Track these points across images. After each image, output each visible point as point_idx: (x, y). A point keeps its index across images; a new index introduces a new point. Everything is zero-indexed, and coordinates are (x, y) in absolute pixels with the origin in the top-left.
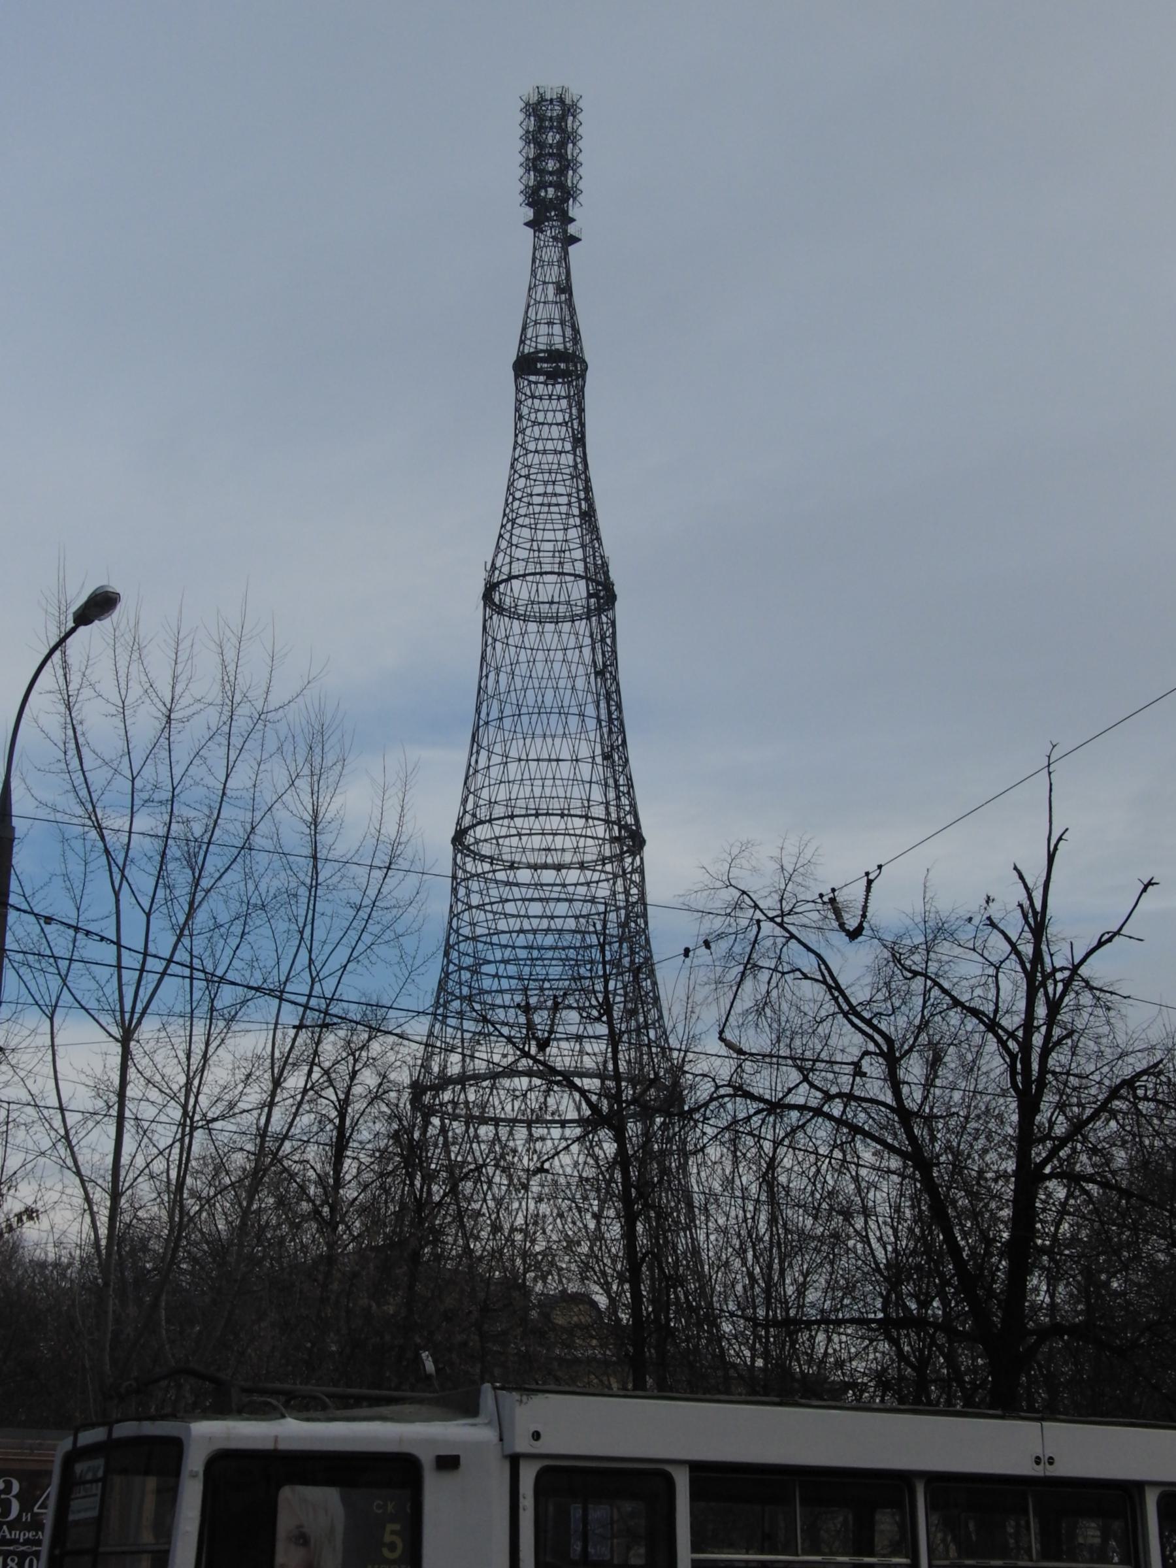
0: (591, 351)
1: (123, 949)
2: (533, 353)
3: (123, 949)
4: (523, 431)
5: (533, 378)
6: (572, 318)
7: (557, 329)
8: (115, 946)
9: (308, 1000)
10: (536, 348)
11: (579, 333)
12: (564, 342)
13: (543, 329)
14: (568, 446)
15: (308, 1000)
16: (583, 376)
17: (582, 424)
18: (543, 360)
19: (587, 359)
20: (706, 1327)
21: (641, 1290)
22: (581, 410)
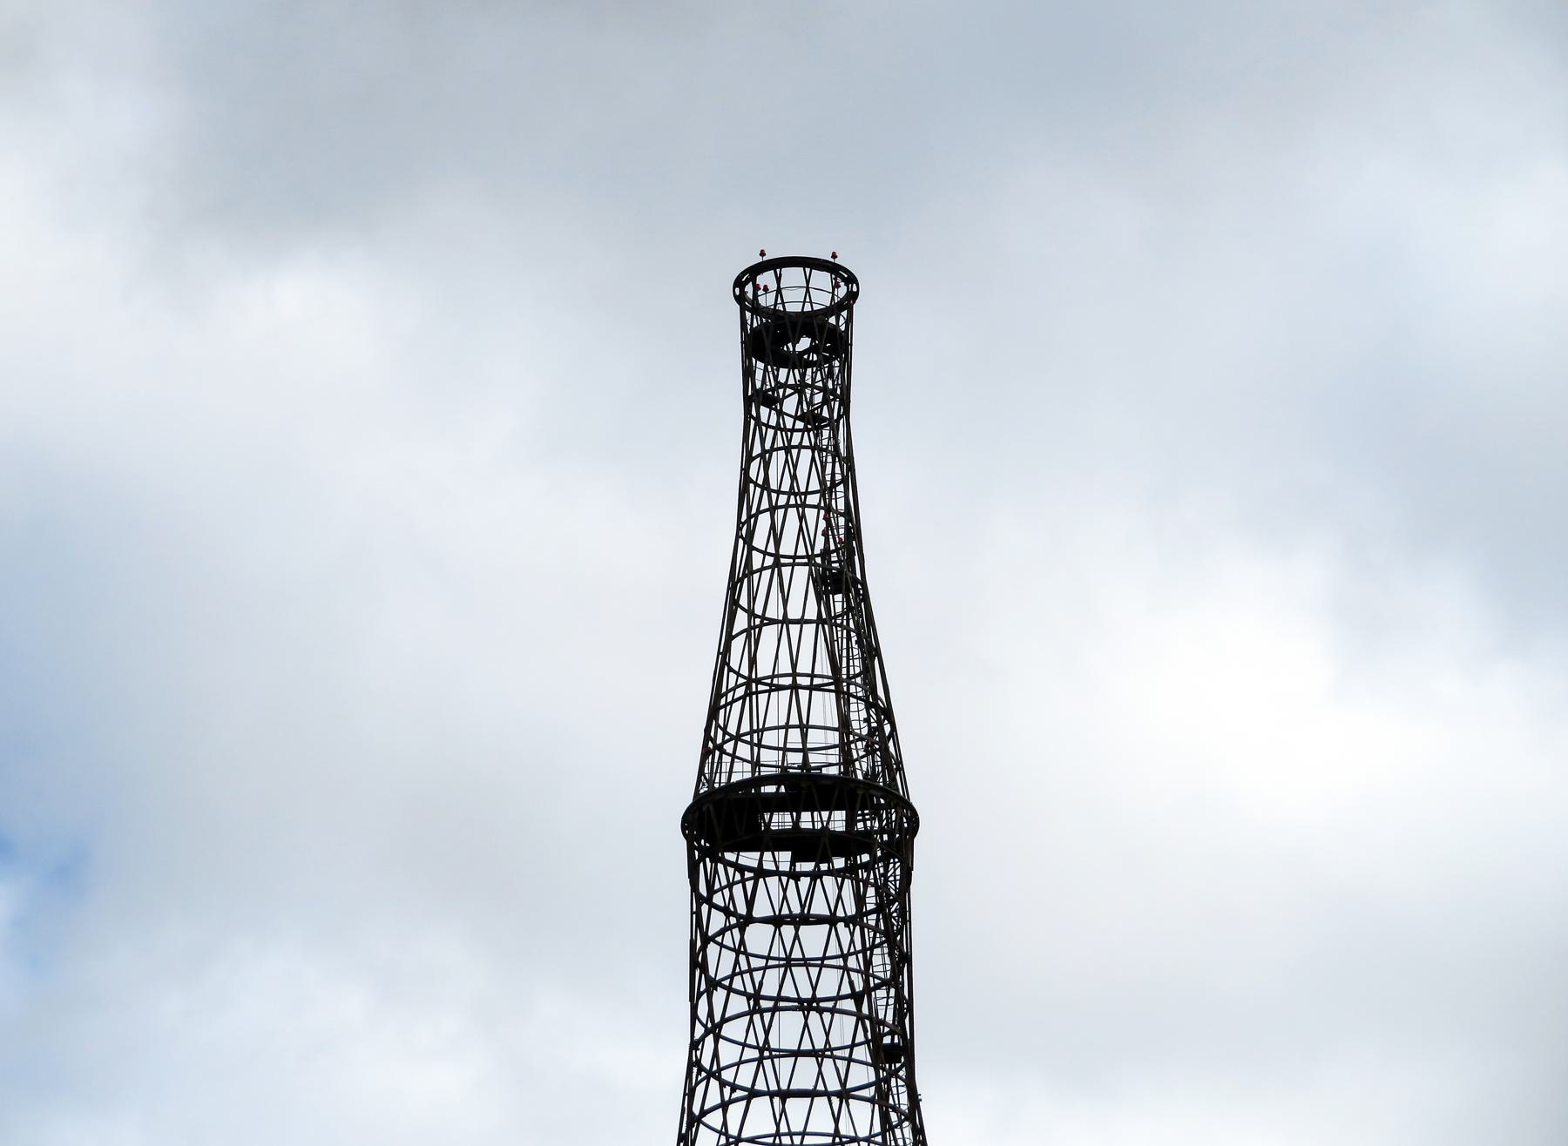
0: (919, 788)
1: (743, 1059)
2: (743, 784)
3: (743, 1059)
4: (715, 1030)
5: (749, 859)
6: (867, 672)
7: (824, 708)
8: (821, 956)
9: (785, 1134)
10: (756, 764)
11: (900, 768)
12: (845, 748)
13: (776, 707)
14: (861, 1075)
15: (785, 1134)
16: (900, 846)
17: (904, 1007)
18: (777, 804)
19: (914, 801)
20: (828, 345)
21: (900, 875)
22: (902, 959)
